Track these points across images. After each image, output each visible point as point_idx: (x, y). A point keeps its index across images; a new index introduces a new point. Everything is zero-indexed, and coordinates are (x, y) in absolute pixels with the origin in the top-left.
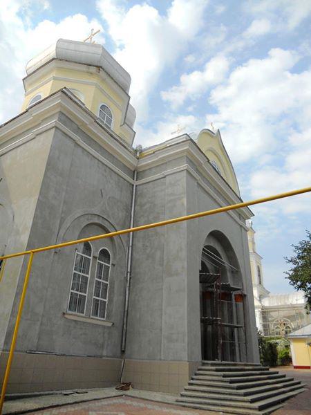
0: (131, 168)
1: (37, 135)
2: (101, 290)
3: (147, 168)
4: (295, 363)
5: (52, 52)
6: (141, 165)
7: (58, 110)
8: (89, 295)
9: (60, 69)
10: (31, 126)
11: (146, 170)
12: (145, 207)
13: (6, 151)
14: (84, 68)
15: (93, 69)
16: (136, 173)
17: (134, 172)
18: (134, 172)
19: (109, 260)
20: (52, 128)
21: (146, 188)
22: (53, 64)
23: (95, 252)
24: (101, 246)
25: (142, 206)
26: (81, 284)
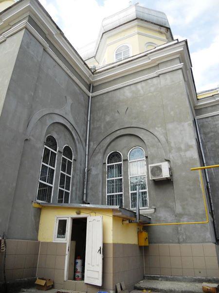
0: (87, 82)
1: (8, 37)
2: (65, 181)
3: (203, 107)
4: (86, 280)
5: (132, 14)
6: (199, 104)
7: (28, 14)
8: (55, 186)
9: (139, 26)
10: (72, 50)
11: (201, 109)
12: (210, 135)
13: (122, 86)
14: (157, 28)
15: (163, 30)
16: (91, 87)
17: (89, 88)
18: (90, 85)
19: (72, 157)
20: (21, 30)
21: (207, 122)
22: (136, 22)
23: (61, 147)
24: (65, 145)
25: (205, 134)
26: (48, 174)
